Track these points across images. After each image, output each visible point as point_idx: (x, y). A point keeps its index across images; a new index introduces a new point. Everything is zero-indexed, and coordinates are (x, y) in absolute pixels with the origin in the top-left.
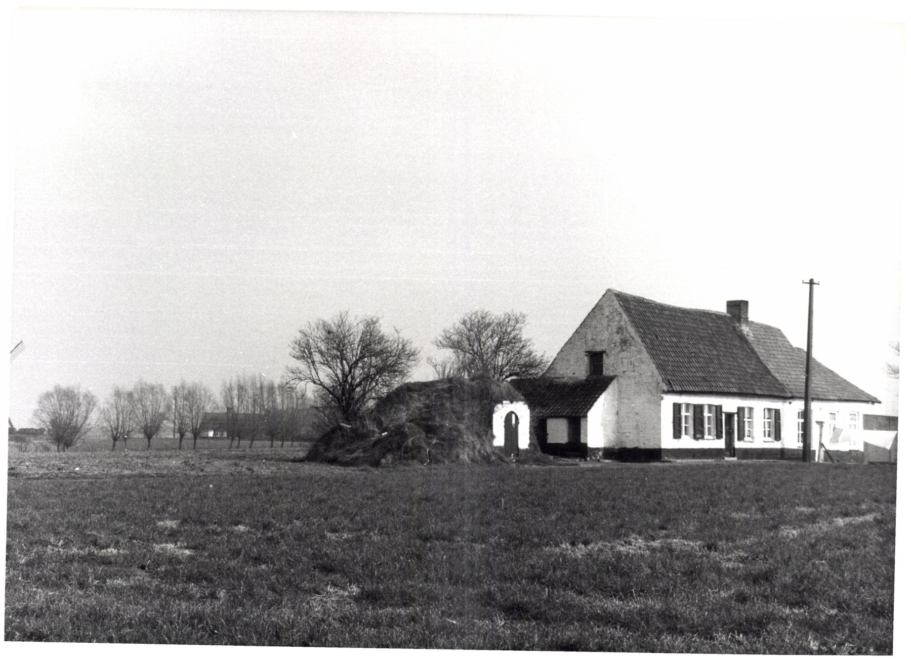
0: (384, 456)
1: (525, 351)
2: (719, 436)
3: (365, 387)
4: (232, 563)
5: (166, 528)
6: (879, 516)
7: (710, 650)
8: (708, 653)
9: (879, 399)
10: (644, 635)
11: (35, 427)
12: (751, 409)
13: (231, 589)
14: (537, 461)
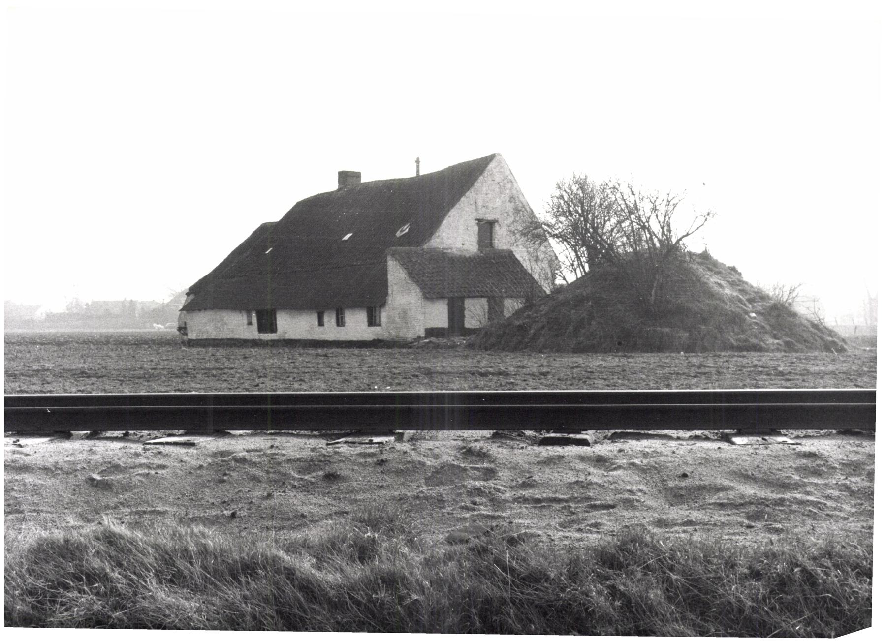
7: (614, 632)
8: (612, 635)
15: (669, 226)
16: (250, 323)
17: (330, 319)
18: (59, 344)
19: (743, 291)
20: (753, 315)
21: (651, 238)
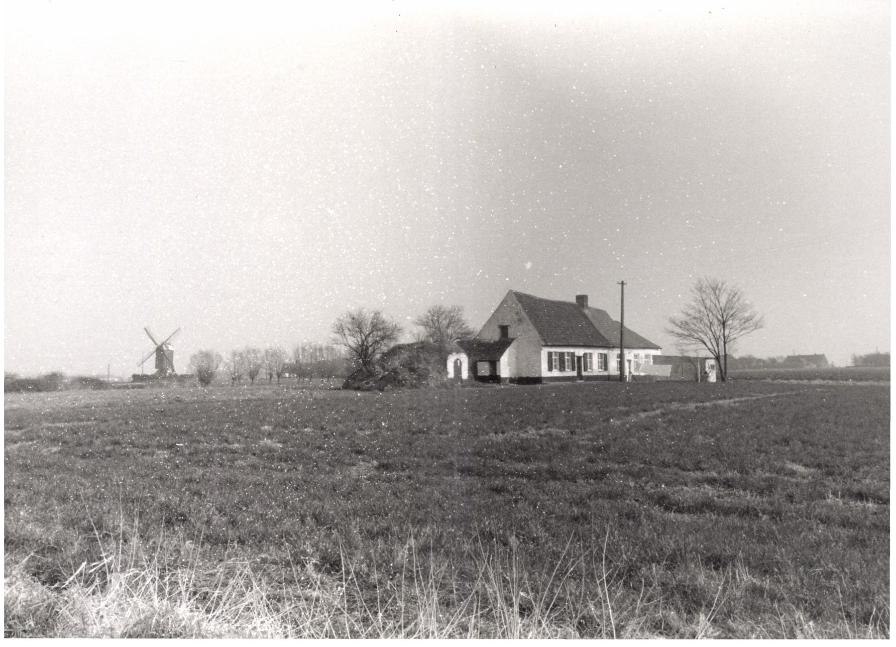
0: (386, 385)
1: (464, 326)
2: (573, 369)
3: (374, 347)
4: (305, 451)
5: (266, 431)
6: (664, 411)
9: (661, 347)
10: (538, 482)
11: (189, 373)
12: (591, 354)
13: (305, 464)
14: (473, 386)
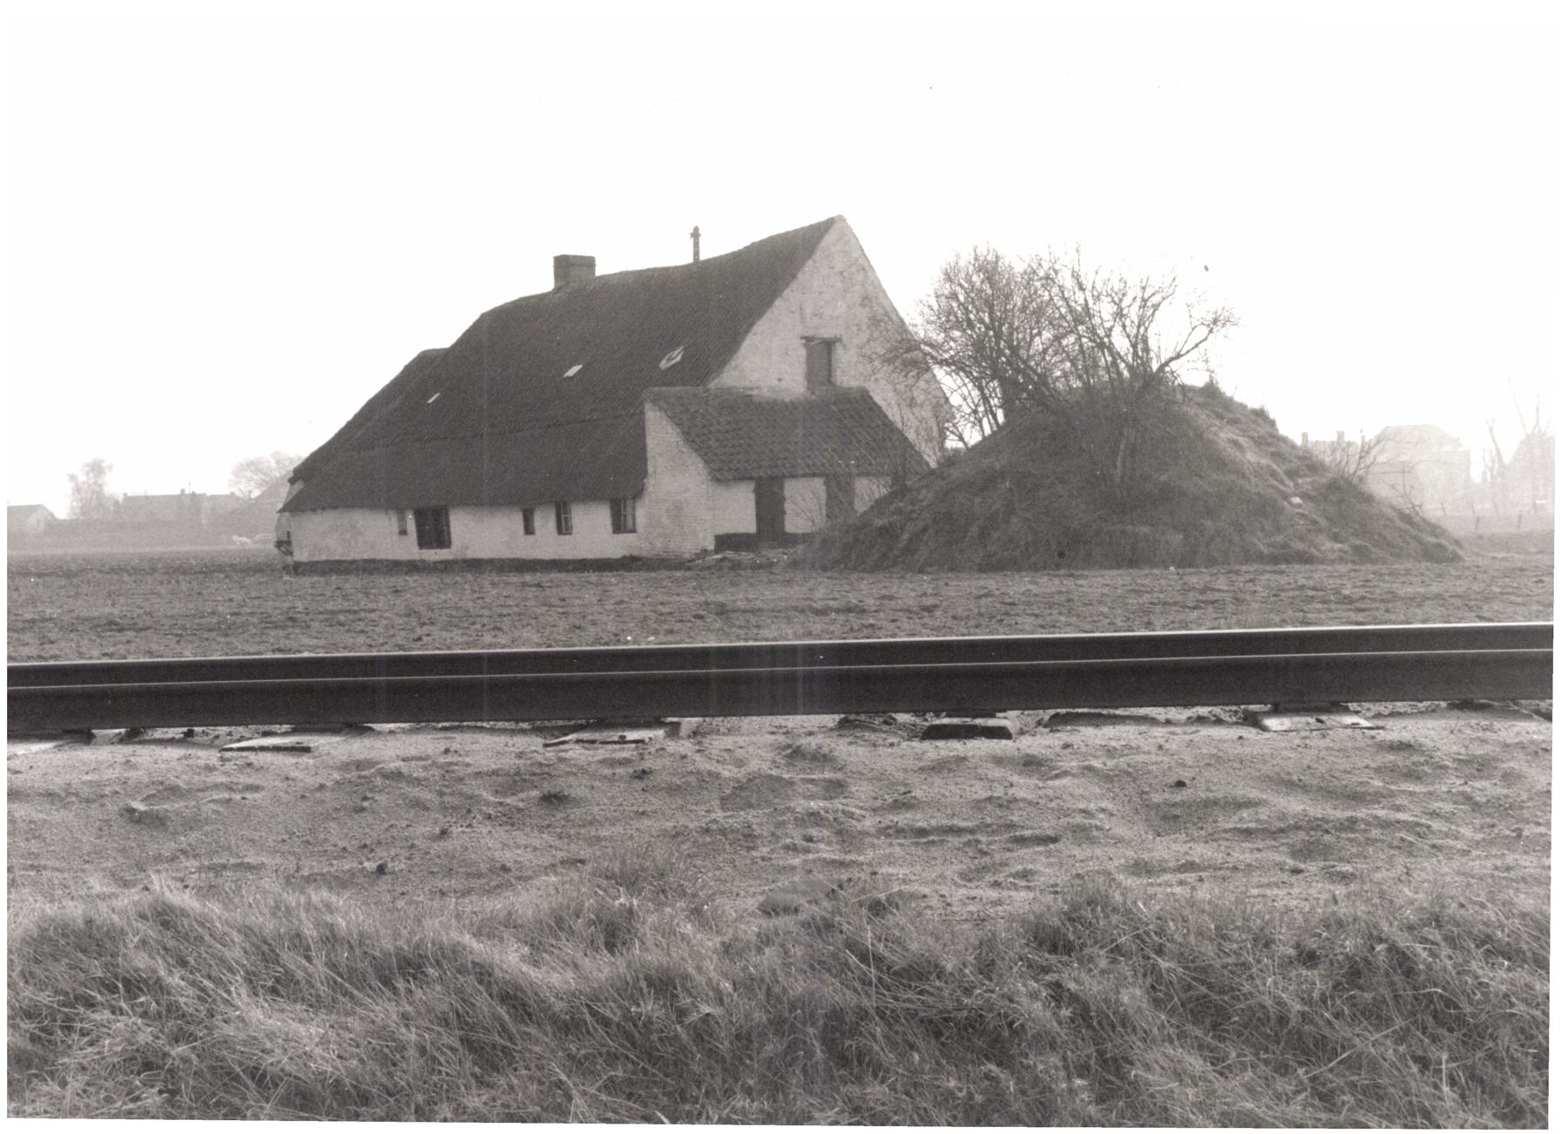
15: (1145, 341)
16: (403, 532)
17: (545, 521)
18: (69, 575)
19: (1277, 456)
20: (1297, 500)
21: (1114, 364)
